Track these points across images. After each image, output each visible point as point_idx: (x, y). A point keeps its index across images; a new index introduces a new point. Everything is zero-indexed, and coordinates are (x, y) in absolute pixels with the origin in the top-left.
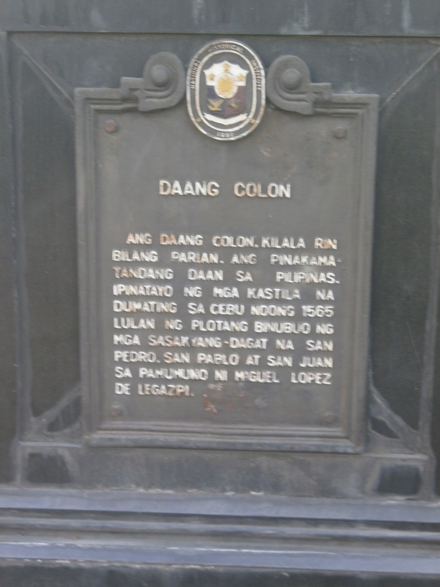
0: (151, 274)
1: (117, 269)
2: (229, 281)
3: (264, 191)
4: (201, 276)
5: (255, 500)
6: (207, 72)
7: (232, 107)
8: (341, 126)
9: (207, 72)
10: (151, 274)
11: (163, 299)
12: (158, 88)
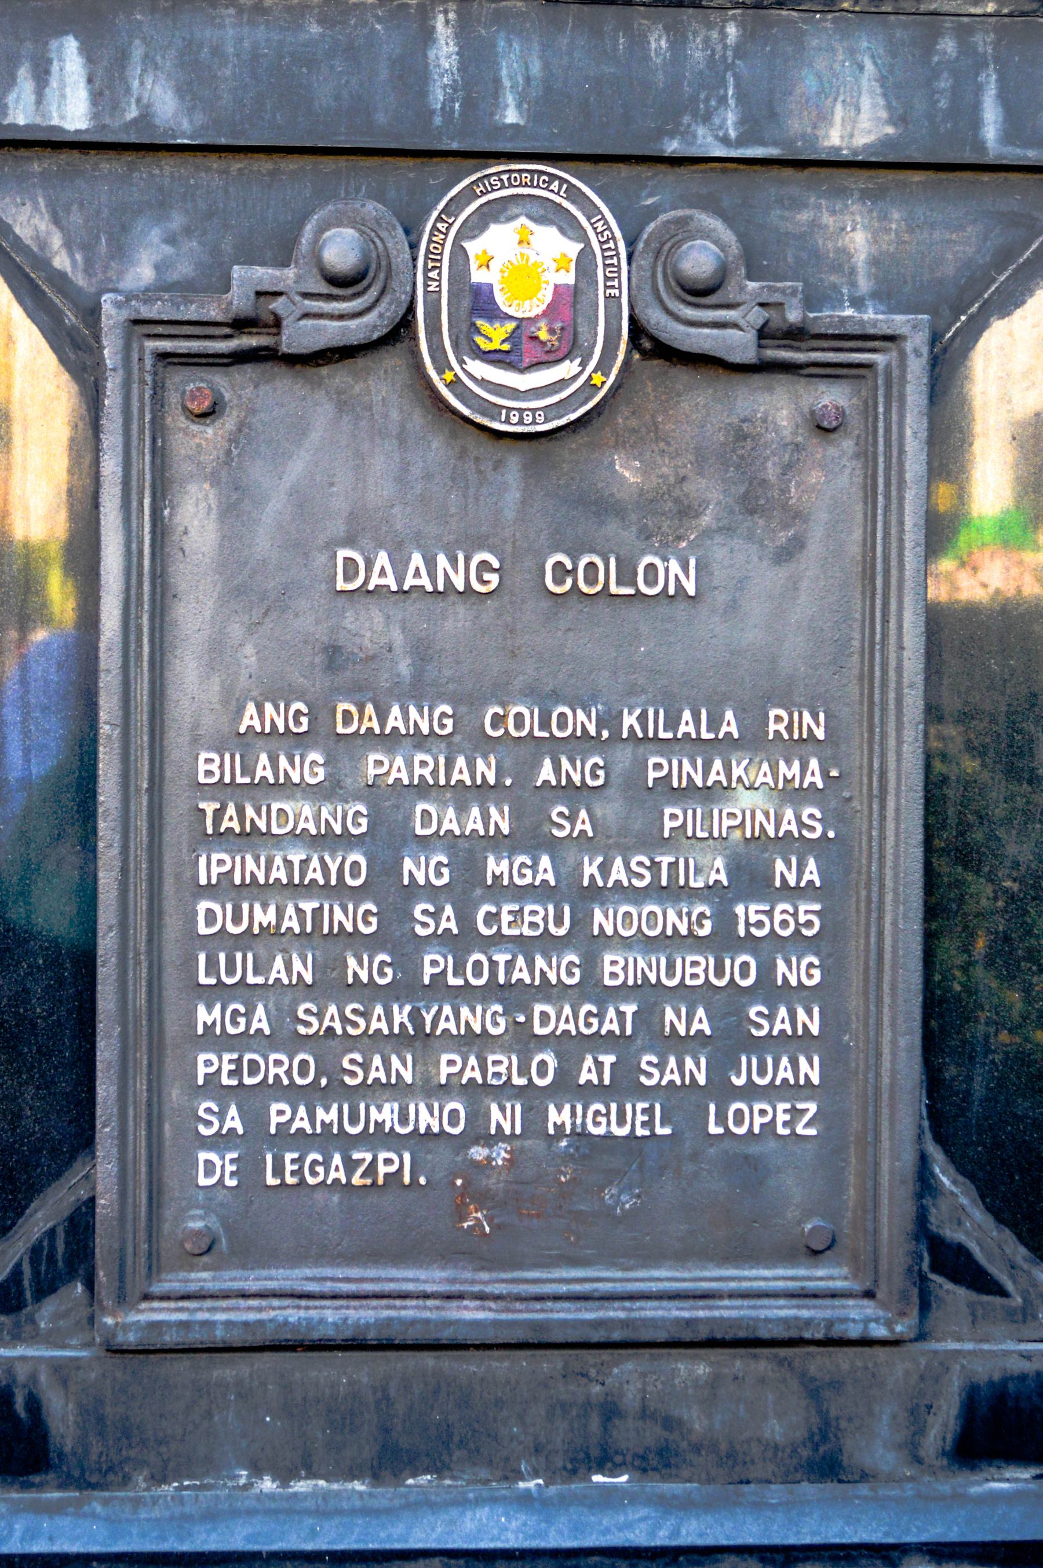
0: (304, 814)
1: (209, 807)
2: (530, 837)
3: (627, 576)
4: (450, 823)
5: (608, 1498)
6: (472, 247)
7: (543, 344)
8: (831, 396)
9: (472, 247)
10: (304, 814)
11: (337, 891)
12: (336, 291)
